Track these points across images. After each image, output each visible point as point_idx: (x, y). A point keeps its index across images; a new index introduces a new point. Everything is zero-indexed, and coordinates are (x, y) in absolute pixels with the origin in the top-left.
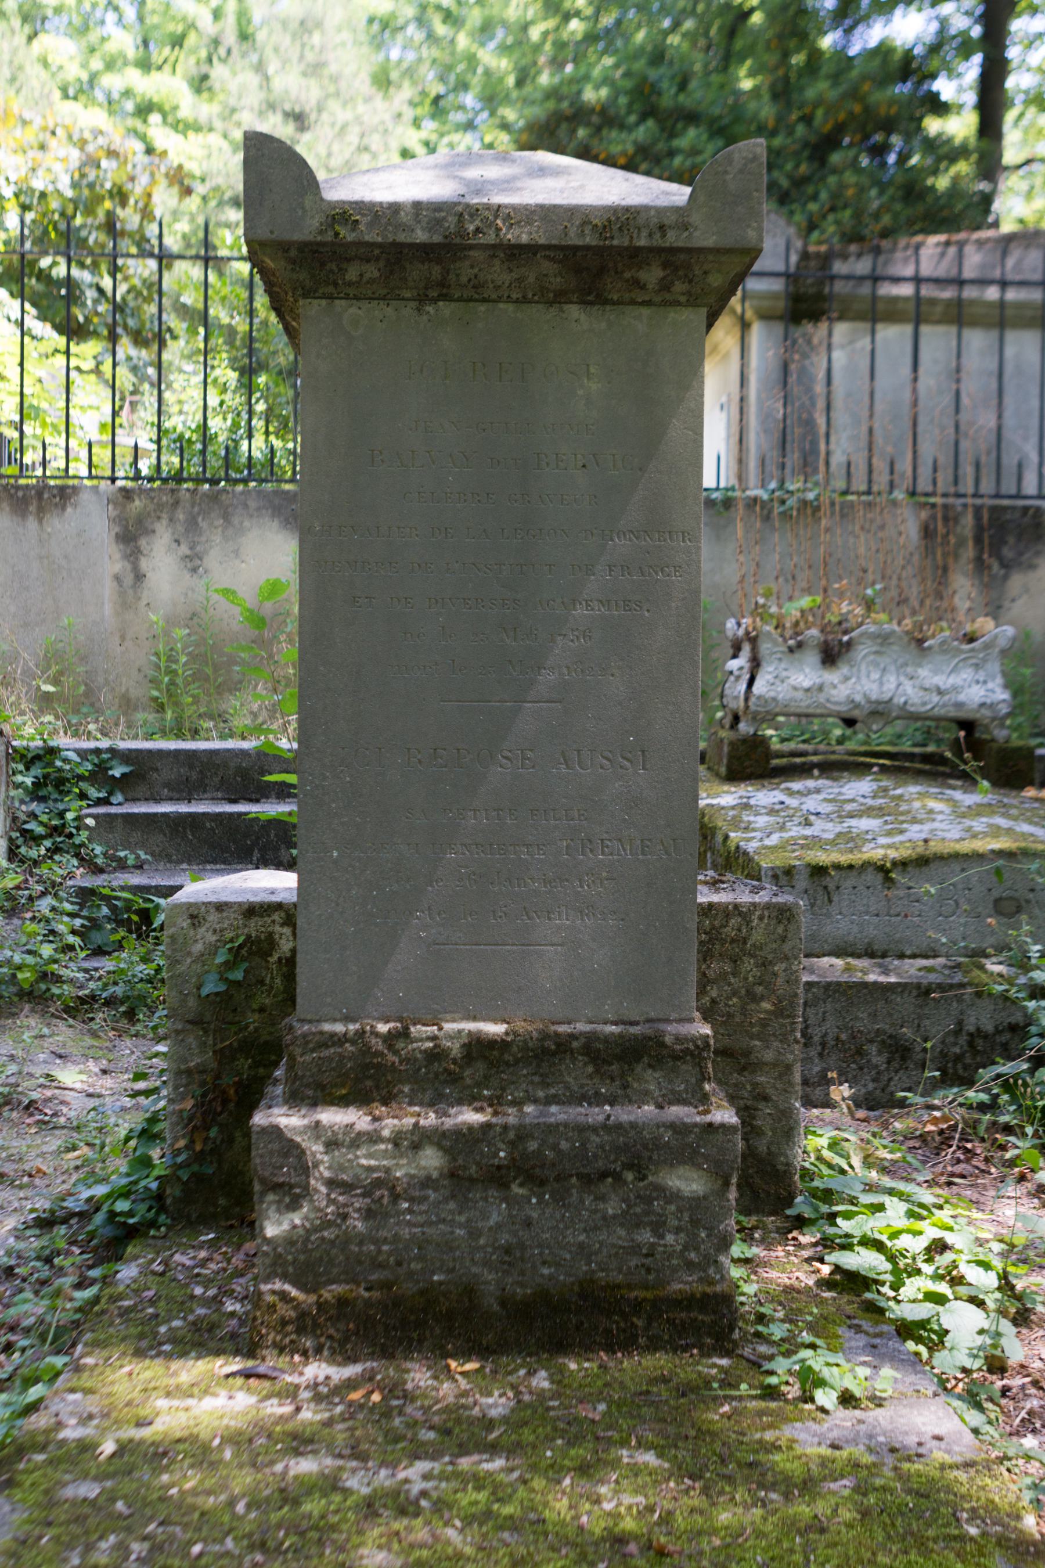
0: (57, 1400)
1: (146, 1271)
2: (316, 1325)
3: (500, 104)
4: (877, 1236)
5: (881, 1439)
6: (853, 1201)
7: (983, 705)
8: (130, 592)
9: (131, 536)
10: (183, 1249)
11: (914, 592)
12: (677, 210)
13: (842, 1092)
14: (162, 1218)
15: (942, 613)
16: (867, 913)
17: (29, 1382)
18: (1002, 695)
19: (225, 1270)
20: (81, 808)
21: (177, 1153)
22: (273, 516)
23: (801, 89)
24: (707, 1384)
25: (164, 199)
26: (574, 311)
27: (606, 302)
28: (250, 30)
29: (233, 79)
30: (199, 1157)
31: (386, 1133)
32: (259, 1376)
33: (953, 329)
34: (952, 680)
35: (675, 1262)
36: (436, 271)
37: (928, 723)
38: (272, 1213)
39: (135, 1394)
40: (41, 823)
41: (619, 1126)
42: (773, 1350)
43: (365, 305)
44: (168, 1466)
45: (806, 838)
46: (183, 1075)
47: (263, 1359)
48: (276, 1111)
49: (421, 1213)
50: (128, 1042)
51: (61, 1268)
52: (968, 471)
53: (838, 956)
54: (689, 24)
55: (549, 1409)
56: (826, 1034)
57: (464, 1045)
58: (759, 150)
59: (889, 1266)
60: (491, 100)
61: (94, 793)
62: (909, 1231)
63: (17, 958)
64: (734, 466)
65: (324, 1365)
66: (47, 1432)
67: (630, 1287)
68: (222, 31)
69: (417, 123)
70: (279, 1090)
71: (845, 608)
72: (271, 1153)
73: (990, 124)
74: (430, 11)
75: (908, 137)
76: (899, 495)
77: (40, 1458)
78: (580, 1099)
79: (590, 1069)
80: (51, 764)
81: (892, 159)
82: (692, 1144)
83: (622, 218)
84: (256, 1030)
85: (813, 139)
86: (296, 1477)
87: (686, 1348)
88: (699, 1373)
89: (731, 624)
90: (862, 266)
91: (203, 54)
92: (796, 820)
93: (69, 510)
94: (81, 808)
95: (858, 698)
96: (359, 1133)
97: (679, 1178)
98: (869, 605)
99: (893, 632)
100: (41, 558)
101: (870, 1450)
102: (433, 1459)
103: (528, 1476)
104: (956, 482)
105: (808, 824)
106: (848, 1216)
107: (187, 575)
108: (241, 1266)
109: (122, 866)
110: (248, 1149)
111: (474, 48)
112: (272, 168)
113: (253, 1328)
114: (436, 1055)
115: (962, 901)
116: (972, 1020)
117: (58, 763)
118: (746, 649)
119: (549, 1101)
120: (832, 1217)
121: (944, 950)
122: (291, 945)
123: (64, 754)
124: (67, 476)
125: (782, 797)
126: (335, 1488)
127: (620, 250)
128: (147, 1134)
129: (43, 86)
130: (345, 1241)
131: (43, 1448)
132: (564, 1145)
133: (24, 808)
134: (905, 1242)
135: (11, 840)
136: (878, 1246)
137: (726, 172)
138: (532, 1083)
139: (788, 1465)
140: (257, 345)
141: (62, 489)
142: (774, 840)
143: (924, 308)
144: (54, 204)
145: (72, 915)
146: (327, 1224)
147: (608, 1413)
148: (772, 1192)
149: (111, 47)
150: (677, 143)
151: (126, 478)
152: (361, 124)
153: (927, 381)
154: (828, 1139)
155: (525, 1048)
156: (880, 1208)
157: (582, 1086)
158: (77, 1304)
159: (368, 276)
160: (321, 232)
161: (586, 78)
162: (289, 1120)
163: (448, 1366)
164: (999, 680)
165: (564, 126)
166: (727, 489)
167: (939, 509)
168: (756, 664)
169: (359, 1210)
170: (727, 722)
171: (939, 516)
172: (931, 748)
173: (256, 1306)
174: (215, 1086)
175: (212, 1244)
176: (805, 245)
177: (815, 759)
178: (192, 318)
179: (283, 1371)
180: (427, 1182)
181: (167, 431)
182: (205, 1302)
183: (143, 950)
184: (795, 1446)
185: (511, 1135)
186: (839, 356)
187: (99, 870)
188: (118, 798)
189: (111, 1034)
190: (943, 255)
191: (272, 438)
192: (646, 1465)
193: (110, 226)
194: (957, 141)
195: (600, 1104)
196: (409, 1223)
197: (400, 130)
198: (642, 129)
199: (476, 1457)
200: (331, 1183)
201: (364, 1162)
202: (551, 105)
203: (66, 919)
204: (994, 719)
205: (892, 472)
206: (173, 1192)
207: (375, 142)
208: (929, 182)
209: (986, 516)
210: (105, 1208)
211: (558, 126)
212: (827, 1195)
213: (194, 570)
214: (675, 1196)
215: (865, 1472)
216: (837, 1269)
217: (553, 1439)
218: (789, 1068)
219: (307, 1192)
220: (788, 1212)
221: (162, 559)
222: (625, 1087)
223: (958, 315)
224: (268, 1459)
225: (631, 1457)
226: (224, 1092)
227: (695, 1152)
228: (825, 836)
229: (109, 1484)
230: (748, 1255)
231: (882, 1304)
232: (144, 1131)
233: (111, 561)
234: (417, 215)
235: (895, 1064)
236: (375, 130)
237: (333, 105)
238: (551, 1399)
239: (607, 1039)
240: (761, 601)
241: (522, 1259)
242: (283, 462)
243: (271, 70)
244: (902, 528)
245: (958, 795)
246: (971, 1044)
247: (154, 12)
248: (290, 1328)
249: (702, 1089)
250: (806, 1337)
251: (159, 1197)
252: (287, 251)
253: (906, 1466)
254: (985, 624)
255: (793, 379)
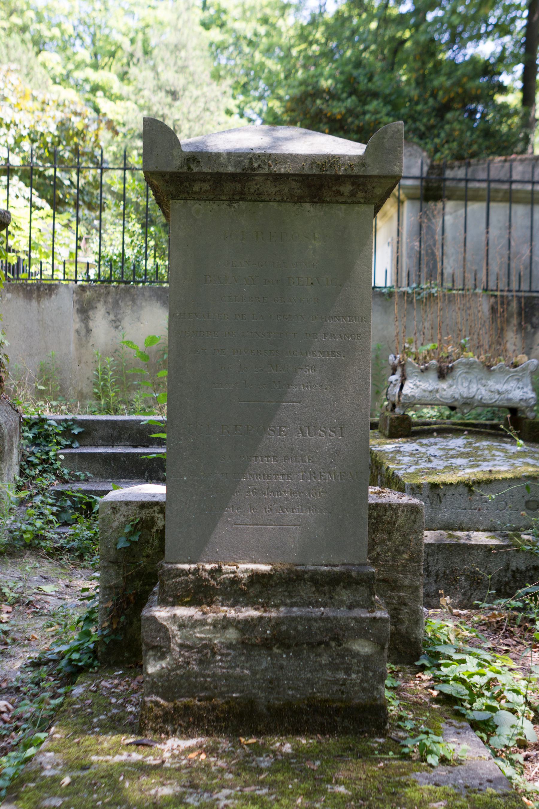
0: (41, 756)
1: (87, 690)
2: (173, 719)
3: (276, 87)
4: (462, 676)
5: (461, 781)
6: (450, 658)
7: (521, 400)
8: (84, 338)
9: (84, 310)
10: (106, 678)
11: (486, 341)
12: (359, 157)
13: (446, 600)
14: (96, 663)
15: (501, 352)
16: (460, 508)
17: (27, 746)
18: (531, 395)
19: (127, 690)
20: (57, 450)
21: (104, 629)
22: (157, 300)
23: (431, 81)
24: (372, 751)
25: (105, 135)
26: (307, 206)
27: (323, 202)
28: (149, 49)
29: (140, 73)
30: (115, 632)
31: (209, 621)
32: (144, 745)
33: (507, 205)
34: (505, 387)
35: (356, 688)
36: (238, 187)
37: (494, 409)
38: (152, 662)
39: (81, 753)
40: (37, 457)
41: (328, 618)
42: (407, 735)
43: (202, 203)
44: (97, 790)
45: (429, 469)
46: (107, 589)
47: (146, 736)
48: (154, 609)
49: (227, 662)
50: (80, 571)
51: (44, 688)
52: (514, 279)
53: (444, 530)
54: (373, 47)
55: (290, 763)
56: (438, 571)
57: (249, 576)
58: (400, 127)
59: (467, 692)
60: (272, 86)
61: (64, 442)
62: (478, 674)
63: (24, 527)
64: (394, 278)
65: (177, 739)
66: (36, 772)
67: (333, 701)
68: (135, 50)
69: (234, 97)
70: (156, 598)
71: (450, 349)
72: (151, 630)
73: (528, 99)
74: (241, 39)
75: (486, 106)
76: (479, 291)
77: (32, 785)
78: (309, 604)
79: (314, 589)
80: (42, 427)
81: (478, 116)
82: (363, 629)
83: (331, 161)
84: (145, 566)
85: (437, 105)
86: (161, 797)
87: (362, 733)
88: (368, 746)
89: (391, 357)
90: (460, 173)
91: (125, 60)
92: (424, 459)
93: (53, 296)
94: (57, 450)
95: (457, 396)
96: (196, 621)
97: (359, 645)
98: (463, 348)
99: (475, 362)
100: (39, 321)
101: (455, 787)
102: (231, 788)
103: (279, 798)
104: (509, 285)
105: (430, 461)
106: (447, 666)
107: (113, 330)
108: (135, 688)
109: (78, 479)
110: (140, 628)
111: (264, 59)
112: (156, 134)
113: (141, 720)
114: (235, 581)
115: (509, 502)
116: (514, 564)
117: (46, 427)
118: (399, 370)
119: (292, 605)
120: (438, 666)
121: (499, 528)
122: (163, 523)
123: (49, 422)
124: (53, 279)
125: (417, 447)
126: (181, 803)
127: (331, 177)
128: (89, 619)
129: (43, 77)
130: (188, 676)
131: (34, 780)
132: (300, 628)
133: (28, 449)
134: (476, 679)
135: (21, 466)
136: (463, 681)
137: (384, 138)
138: (284, 595)
139: (412, 794)
140: (150, 212)
141: (50, 286)
142: (412, 470)
143: (492, 194)
144: (49, 139)
145: (52, 505)
146: (179, 667)
147: (321, 766)
148: (411, 651)
149: (78, 58)
150: (367, 108)
151: (83, 280)
152: (205, 97)
153: (494, 232)
154: (442, 624)
155: (280, 578)
156: (463, 661)
157: (309, 598)
158: (51, 707)
159: (204, 188)
160: (181, 167)
161: (321, 75)
162: (161, 613)
163: (240, 741)
164: (530, 387)
165: (309, 99)
166: (390, 287)
167: (499, 298)
168: (404, 378)
169: (195, 660)
170: (389, 408)
171: (499, 302)
172: (495, 422)
173: (143, 708)
174: (124, 595)
175: (121, 676)
176: (432, 161)
177: (434, 427)
178: (117, 197)
179: (156, 742)
180: (230, 646)
181: (104, 257)
182: (117, 706)
183: (88, 524)
184: (417, 784)
185: (273, 622)
186: (448, 218)
187: (66, 482)
188: (76, 444)
189: (71, 567)
190: (503, 167)
191: (157, 259)
192: (340, 793)
193: (76, 152)
194: (512, 106)
195: (319, 607)
196: (221, 667)
197: (225, 100)
198: (349, 100)
199: (253, 788)
200: (181, 646)
201: (198, 635)
202: (303, 88)
203: (49, 507)
204: (527, 407)
205: (475, 280)
206: (101, 649)
207: (212, 106)
208: (497, 128)
209: (523, 300)
210: (67, 657)
211: (306, 99)
212: (437, 655)
213: (117, 327)
214: (357, 655)
215: (452, 798)
216: (441, 693)
217: (293, 779)
218: (417, 588)
219: (169, 650)
220: (416, 663)
221: (100, 321)
222: (331, 598)
223: (510, 198)
224: (147, 787)
225: (332, 788)
226: (128, 598)
227: (367, 632)
228: (439, 468)
229: (67, 799)
230: (395, 685)
231: (464, 712)
232: (87, 618)
233: (74, 323)
234: (229, 159)
235: (474, 586)
236: (213, 100)
237: (191, 87)
238: (292, 758)
239: (322, 574)
240: (407, 345)
241: (278, 686)
242: (163, 272)
243: (160, 69)
244: (480, 308)
245: (508, 446)
246: (513, 576)
247: (99, 40)
248: (160, 720)
249: (370, 600)
250: (423, 728)
251: (94, 652)
252: (164, 176)
253: (473, 795)
254: (522, 358)
255: (424, 231)
